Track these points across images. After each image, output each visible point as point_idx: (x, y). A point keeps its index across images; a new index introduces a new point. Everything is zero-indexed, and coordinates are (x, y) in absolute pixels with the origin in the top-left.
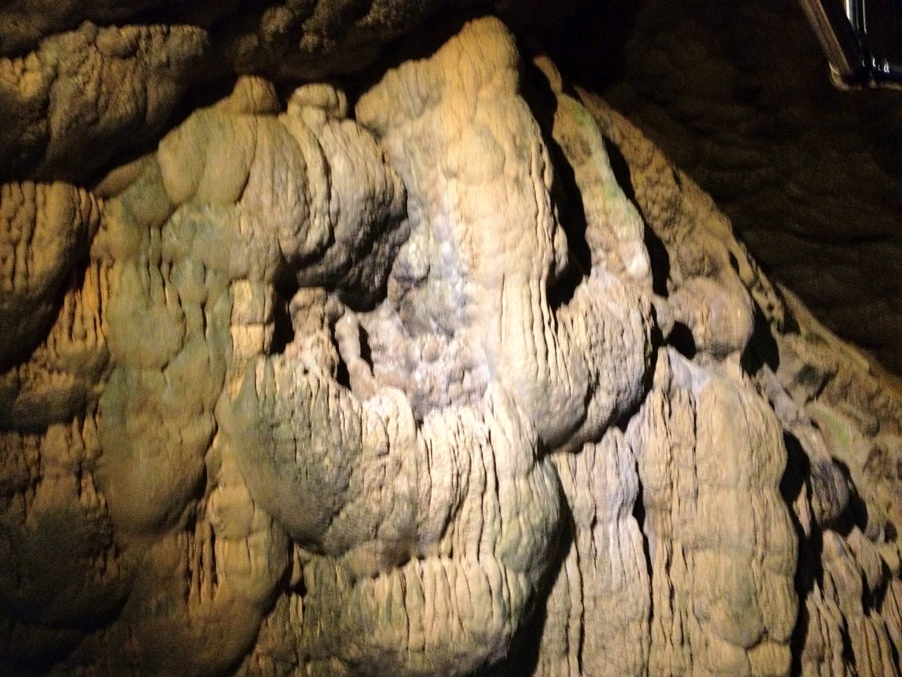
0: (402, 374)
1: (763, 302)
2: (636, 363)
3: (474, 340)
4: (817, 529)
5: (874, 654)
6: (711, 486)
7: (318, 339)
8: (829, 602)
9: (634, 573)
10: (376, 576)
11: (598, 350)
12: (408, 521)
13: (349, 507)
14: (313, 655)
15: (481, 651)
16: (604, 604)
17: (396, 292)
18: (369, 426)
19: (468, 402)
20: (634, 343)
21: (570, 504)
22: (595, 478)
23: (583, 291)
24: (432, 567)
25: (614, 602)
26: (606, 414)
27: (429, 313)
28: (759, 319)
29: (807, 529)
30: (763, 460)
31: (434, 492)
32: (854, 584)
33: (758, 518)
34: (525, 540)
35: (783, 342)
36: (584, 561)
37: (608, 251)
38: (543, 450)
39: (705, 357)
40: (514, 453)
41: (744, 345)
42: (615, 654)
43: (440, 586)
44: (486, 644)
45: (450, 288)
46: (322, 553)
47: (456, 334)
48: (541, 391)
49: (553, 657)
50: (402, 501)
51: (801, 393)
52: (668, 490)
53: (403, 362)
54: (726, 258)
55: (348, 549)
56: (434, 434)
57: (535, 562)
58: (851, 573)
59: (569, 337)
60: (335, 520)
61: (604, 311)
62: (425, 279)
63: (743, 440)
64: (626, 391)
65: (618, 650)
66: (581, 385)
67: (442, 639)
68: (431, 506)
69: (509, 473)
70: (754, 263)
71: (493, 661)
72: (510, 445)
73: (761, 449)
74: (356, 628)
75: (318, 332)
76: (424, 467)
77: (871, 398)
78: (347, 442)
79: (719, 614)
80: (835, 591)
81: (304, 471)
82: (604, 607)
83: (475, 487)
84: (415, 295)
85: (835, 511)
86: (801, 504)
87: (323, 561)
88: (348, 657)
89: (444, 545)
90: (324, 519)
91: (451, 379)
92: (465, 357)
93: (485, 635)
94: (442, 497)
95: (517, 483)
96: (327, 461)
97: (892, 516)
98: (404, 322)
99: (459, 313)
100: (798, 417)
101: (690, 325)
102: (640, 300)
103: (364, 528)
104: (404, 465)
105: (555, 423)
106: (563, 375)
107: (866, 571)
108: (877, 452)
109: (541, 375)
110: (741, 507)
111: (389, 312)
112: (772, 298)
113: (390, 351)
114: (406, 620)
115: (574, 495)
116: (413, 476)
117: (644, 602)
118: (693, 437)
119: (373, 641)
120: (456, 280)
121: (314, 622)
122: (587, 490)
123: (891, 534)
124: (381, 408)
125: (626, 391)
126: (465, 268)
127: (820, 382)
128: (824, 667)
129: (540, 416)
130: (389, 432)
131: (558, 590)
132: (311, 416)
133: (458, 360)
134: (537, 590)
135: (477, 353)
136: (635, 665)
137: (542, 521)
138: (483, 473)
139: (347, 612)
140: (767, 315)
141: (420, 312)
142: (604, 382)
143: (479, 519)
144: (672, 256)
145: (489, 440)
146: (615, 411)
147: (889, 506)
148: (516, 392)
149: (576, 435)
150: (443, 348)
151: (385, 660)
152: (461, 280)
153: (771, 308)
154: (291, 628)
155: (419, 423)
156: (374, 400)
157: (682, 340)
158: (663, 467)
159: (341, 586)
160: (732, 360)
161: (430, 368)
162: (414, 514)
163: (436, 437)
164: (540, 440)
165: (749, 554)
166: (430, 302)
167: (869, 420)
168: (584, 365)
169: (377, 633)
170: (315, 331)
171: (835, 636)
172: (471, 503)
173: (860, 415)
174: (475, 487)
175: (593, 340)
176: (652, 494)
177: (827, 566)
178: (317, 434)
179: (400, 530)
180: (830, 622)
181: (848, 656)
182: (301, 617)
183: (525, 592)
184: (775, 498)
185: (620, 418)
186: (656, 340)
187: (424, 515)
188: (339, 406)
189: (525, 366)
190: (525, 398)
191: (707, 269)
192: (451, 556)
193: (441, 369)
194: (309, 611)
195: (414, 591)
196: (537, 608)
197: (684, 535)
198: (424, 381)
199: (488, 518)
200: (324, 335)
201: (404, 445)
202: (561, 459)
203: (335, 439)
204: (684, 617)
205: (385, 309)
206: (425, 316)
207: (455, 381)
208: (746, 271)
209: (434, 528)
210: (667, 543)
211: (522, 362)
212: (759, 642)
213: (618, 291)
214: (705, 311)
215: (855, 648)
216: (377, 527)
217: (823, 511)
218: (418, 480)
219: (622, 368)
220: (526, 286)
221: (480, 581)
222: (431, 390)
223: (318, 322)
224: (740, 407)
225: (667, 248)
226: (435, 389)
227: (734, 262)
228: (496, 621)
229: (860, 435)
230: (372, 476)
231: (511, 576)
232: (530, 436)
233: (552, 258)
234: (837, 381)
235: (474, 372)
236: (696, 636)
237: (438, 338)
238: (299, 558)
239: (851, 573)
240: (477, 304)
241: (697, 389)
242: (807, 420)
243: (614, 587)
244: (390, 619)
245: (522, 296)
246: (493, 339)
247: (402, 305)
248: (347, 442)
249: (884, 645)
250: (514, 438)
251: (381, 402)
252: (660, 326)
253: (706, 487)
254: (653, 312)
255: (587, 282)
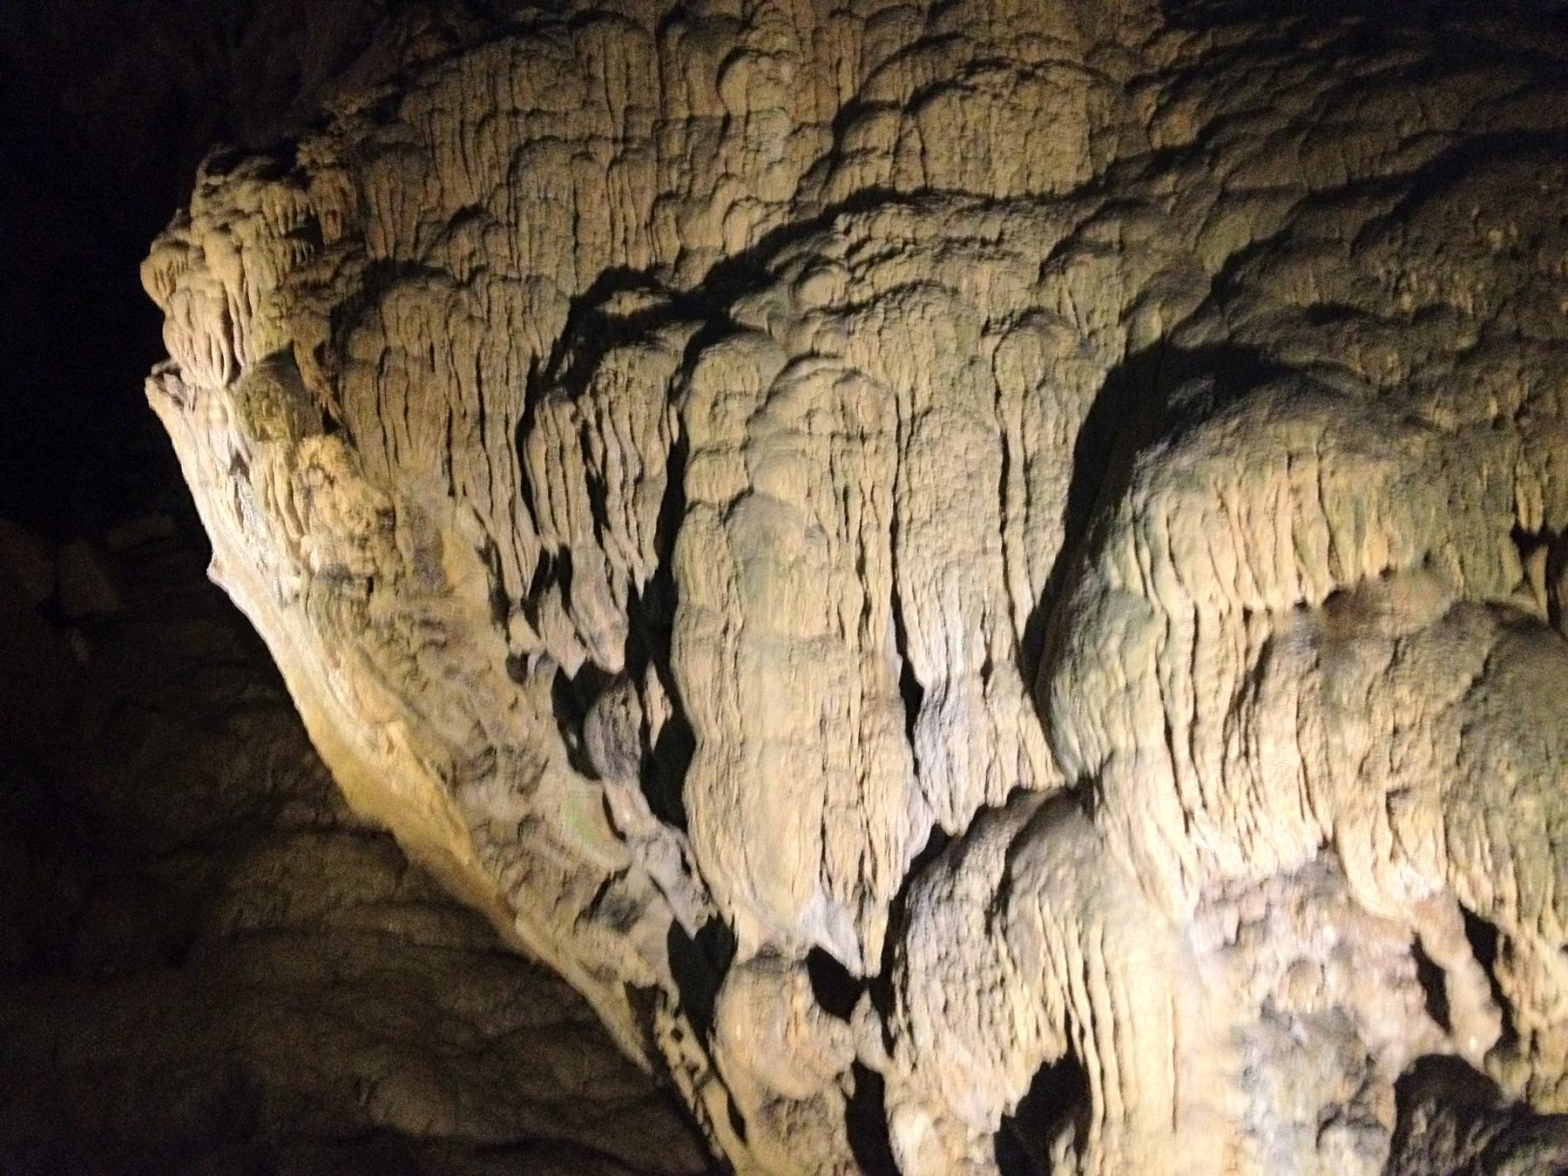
0: (1356, 935)
1: (691, 1047)
2: (922, 950)
3: (1221, 1001)
4: (634, 672)
5: (559, 490)
6: (801, 742)
7: (1544, 1011)
8: (620, 566)
9: (923, 597)
10: (1387, 573)
11: (989, 977)
12: (1339, 674)
13: (1455, 694)
14: (1488, 431)
15: (1184, 461)
16: (971, 544)
17: (1378, 1097)
18: (1432, 847)
19: (1227, 883)
20: (926, 988)
21: (1028, 702)
22: (989, 745)
23: (1016, 1087)
24: (1284, 595)
25: (954, 553)
26: (972, 859)
27: (1312, 1055)
28: (704, 1024)
29: (652, 675)
30: (721, 788)
31: (1291, 726)
32: (585, 591)
33: (731, 695)
34: (1114, 644)
35: (656, 971)
36: (1002, 611)
37: (966, 1160)
38: (1082, 796)
39: (792, 953)
40: (1140, 793)
41: (732, 974)
42: (953, 469)
43: (1267, 565)
44: (1176, 474)
45: (1276, 1105)
46: (1493, 607)
47: (1257, 1012)
48: (1093, 905)
49: (1051, 456)
50: (1352, 708)
51: (635, 885)
52: (866, 732)
53: (1356, 960)
54: (753, 1130)
55: (1446, 619)
56: (1298, 831)
57: (1093, 608)
58: (587, 612)
59: (1045, 1005)
60: (1479, 669)
61: (979, 1049)
62: (1325, 1125)
63: (752, 819)
64: (939, 901)
65: (948, 475)
66: (1021, 915)
67: (1258, 480)
68: (1294, 699)
69: (1148, 759)
70: (700, 1119)
71: (1162, 447)
72: (1146, 803)
73: (723, 803)
74: (1420, 484)
75: (1542, 1024)
76: (1313, 772)
77: (527, 878)
78: (1474, 815)
79: (793, 542)
80: (610, 581)
81: (1554, 761)
82: (971, 541)
83: (1211, 733)
84: (1342, 1091)
85: (606, 702)
86: (660, 714)
87: (1489, 593)
88: (1425, 434)
89: (1261, 633)
90: (1500, 670)
91: (1262, 926)
92: (1237, 970)
93: (1180, 488)
94: (1275, 718)
95: (1132, 742)
96: (1511, 779)
97: (510, 690)
98: (1356, 1036)
99: (1255, 1055)
100: (647, 849)
101: (817, 1010)
102: (914, 1066)
103: (1422, 656)
104: (1356, 772)
105: (1061, 847)
106: (1054, 934)
107: (562, 613)
108: (525, 791)
109: (1095, 934)
110: (758, 712)
111: (1387, 1053)
112: (672, 1051)
113: (1377, 975)
114: (1327, 503)
115: (1022, 718)
116: (1335, 756)
117: (906, 553)
118: (827, 822)
119: (1385, 466)
120: (1266, 1122)
121: (1492, 487)
122: (1000, 727)
123: (518, 667)
124: (1407, 881)
125: (939, 901)
126: (1251, 1144)
127: (604, 904)
128: (634, 471)
129: (1091, 858)
130: (1389, 836)
131: (1046, 561)
132: (1551, 864)
133: (1250, 963)
134: (1086, 562)
135: (1214, 974)
136: (920, 453)
137: (1084, 678)
138: (1198, 759)
139: (1438, 509)
140: (684, 1023)
141: (1328, 1055)
142: (977, 918)
143: (1201, 677)
144: (841, 1136)
145: (1188, 816)
146: (956, 866)
147: (514, 706)
148: (1141, 903)
149: (1024, 821)
150: (1281, 985)
151: (1359, 435)
152: (1257, 1119)
153: (677, 1035)
154: (1538, 475)
155: (1329, 845)
156: (1422, 892)
157: (834, 988)
158: (875, 770)
159: (1450, 549)
160: (750, 946)
161: (1305, 948)
162: (1327, 686)
163: (1292, 824)
164: (1090, 814)
165: (747, 636)
166: (1312, 1078)
167: (533, 841)
168: (1016, 951)
169: (1379, 478)
170: (1550, 1027)
171: (616, 518)
172: (1216, 706)
173: (546, 850)
174: (1211, 733)
175: (998, 995)
176: (892, 725)
177: (620, 617)
178: (1536, 831)
179: (1350, 656)
180: (622, 536)
181: (597, 489)
182: (1520, 496)
183: (1108, 558)
184: (704, 728)
185: (942, 852)
186: (885, 991)
187: (1308, 684)
188: (1496, 883)
189: (1126, 953)
190: (1123, 891)
191: (782, 1111)
192: (1247, 614)
193: (1282, 945)
194: (1505, 501)
195: (1314, 552)
196: (1083, 534)
197: (845, 657)
198: (1318, 925)
199: (1183, 679)
200: (1528, 1019)
201: (1358, 810)
202: (1045, 778)
203: (1500, 823)
204: (843, 533)
205: (1395, 1062)
206: (1318, 1048)
207: (1254, 923)
208: (716, 1103)
209: (1285, 662)
210: (868, 646)
211: (1132, 959)
212: (734, 503)
213: (954, 1084)
214: (792, 1034)
215: (585, 500)
216: (1396, 661)
217: (625, 702)
218: (1326, 746)
219: (945, 941)
220: (1130, 1105)
221: (1193, 577)
222: (1301, 907)
223: (1543, 1044)
224: (755, 874)
225: (849, 1155)
226: (1293, 909)
227: (738, 1124)
228: (1161, 510)
229: (549, 817)
230: (1416, 753)
231: (1136, 584)
232: (1109, 823)
233: (1084, 1161)
234: (579, 902)
235: (1220, 941)
236: (826, 505)
237: (1291, 1006)
238: (1534, 596)
239: (587, 612)
240: (1222, 1074)
241: (817, 901)
242: (633, 844)
243: (955, 572)
244: (1357, 503)
245: (1138, 1087)
246: (1188, 1004)
247: (1363, 1070)
248: (1474, 815)
249: (543, 505)
250: (1140, 821)
251: (1408, 889)
252: (875, 1016)
253: (809, 741)
254: (890, 1043)
255: (1008, 1105)
